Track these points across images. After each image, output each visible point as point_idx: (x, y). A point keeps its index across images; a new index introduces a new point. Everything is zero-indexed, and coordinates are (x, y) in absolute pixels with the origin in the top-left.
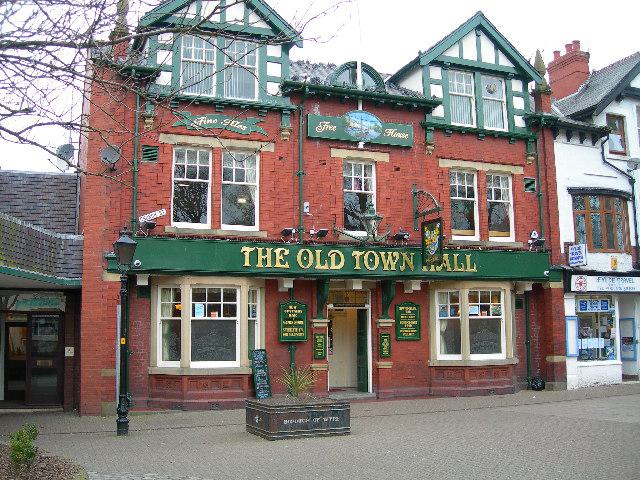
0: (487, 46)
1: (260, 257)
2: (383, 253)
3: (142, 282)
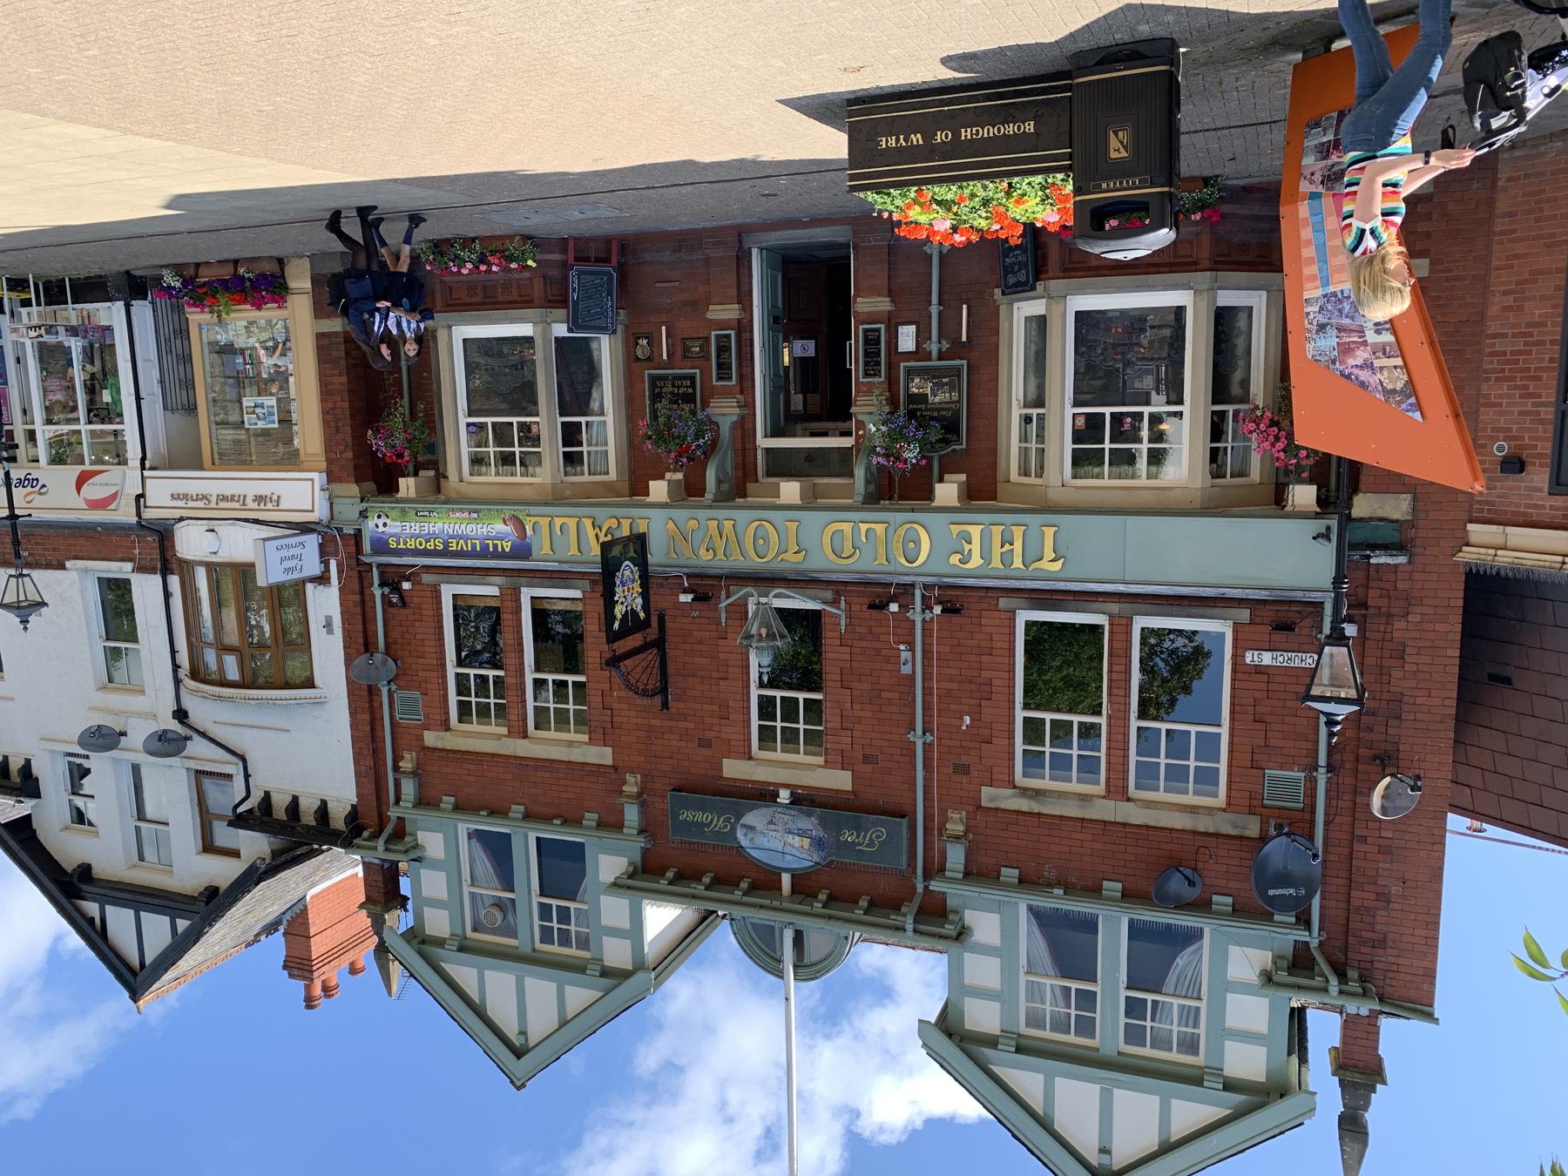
0: (502, 1009)
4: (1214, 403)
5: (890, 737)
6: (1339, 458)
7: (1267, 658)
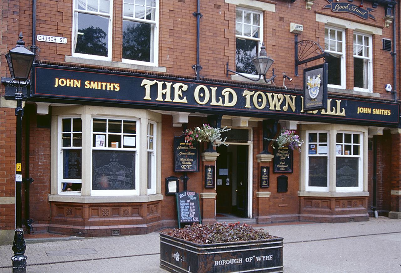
1: (160, 91)
2: (270, 95)
3: (43, 110)
4: (81, 150)
5: (210, 16)
6: (81, 138)
7: (58, 40)
